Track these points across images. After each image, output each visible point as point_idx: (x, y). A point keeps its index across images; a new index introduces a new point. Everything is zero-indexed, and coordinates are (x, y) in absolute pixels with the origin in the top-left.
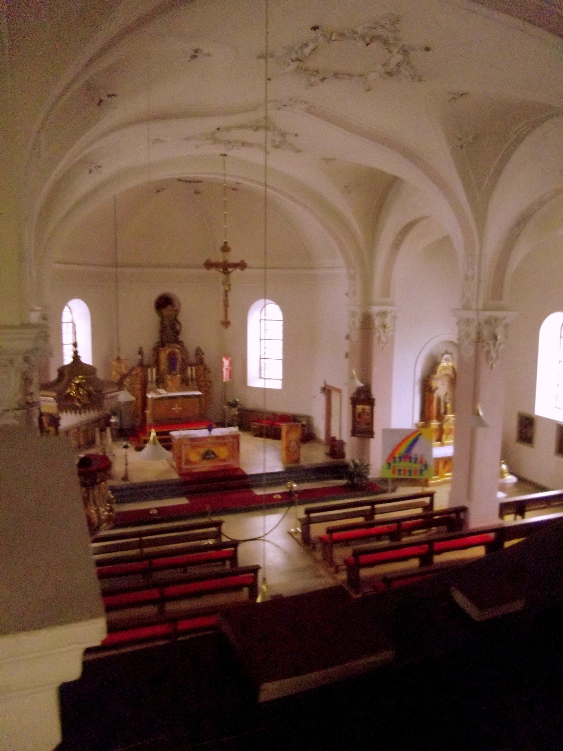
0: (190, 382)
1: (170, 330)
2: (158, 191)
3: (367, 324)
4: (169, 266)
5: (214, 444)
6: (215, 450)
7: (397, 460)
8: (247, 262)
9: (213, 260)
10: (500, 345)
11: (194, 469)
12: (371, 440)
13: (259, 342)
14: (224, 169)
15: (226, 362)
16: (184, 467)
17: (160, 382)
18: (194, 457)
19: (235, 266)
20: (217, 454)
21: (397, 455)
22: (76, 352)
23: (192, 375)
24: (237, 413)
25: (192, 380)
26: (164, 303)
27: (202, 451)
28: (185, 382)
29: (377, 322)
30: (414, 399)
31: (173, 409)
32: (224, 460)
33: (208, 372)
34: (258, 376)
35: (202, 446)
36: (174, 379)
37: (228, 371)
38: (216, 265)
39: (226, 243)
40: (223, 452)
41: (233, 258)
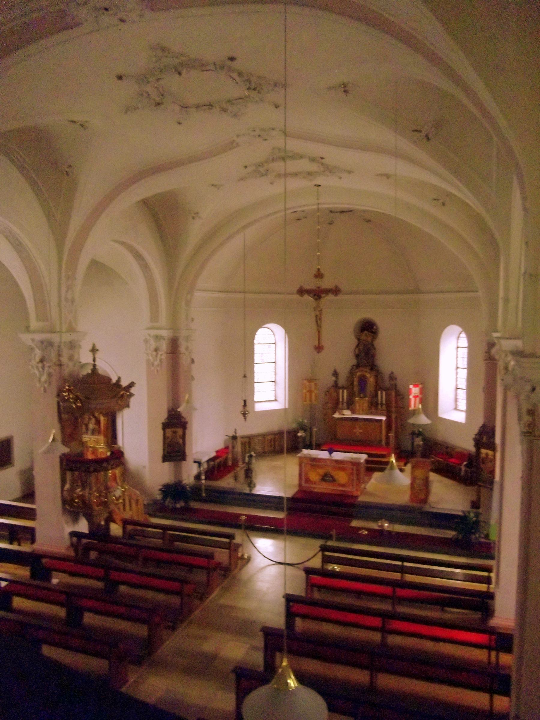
0: (379, 407)
1: (366, 354)
3: (174, 346)
4: (365, 293)
5: (335, 468)
6: (334, 473)
8: (341, 287)
9: (307, 287)
11: (315, 488)
12: (184, 462)
13: (455, 372)
14: (318, 199)
15: (415, 391)
16: (303, 484)
17: (350, 405)
18: (314, 476)
23: (382, 401)
24: (421, 443)
25: (382, 404)
26: (368, 328)
27: (321, 471)
28: (374, 406)
31: (355, 431)
32: (343, 485)
33: (403, 398)
34: (453, 406)
35: (320, 467)
36: (362, 403)
37: (418, 399)
38: (308, 292)
39: (319, 269)
40: (342, 477)
41: (326, 283)
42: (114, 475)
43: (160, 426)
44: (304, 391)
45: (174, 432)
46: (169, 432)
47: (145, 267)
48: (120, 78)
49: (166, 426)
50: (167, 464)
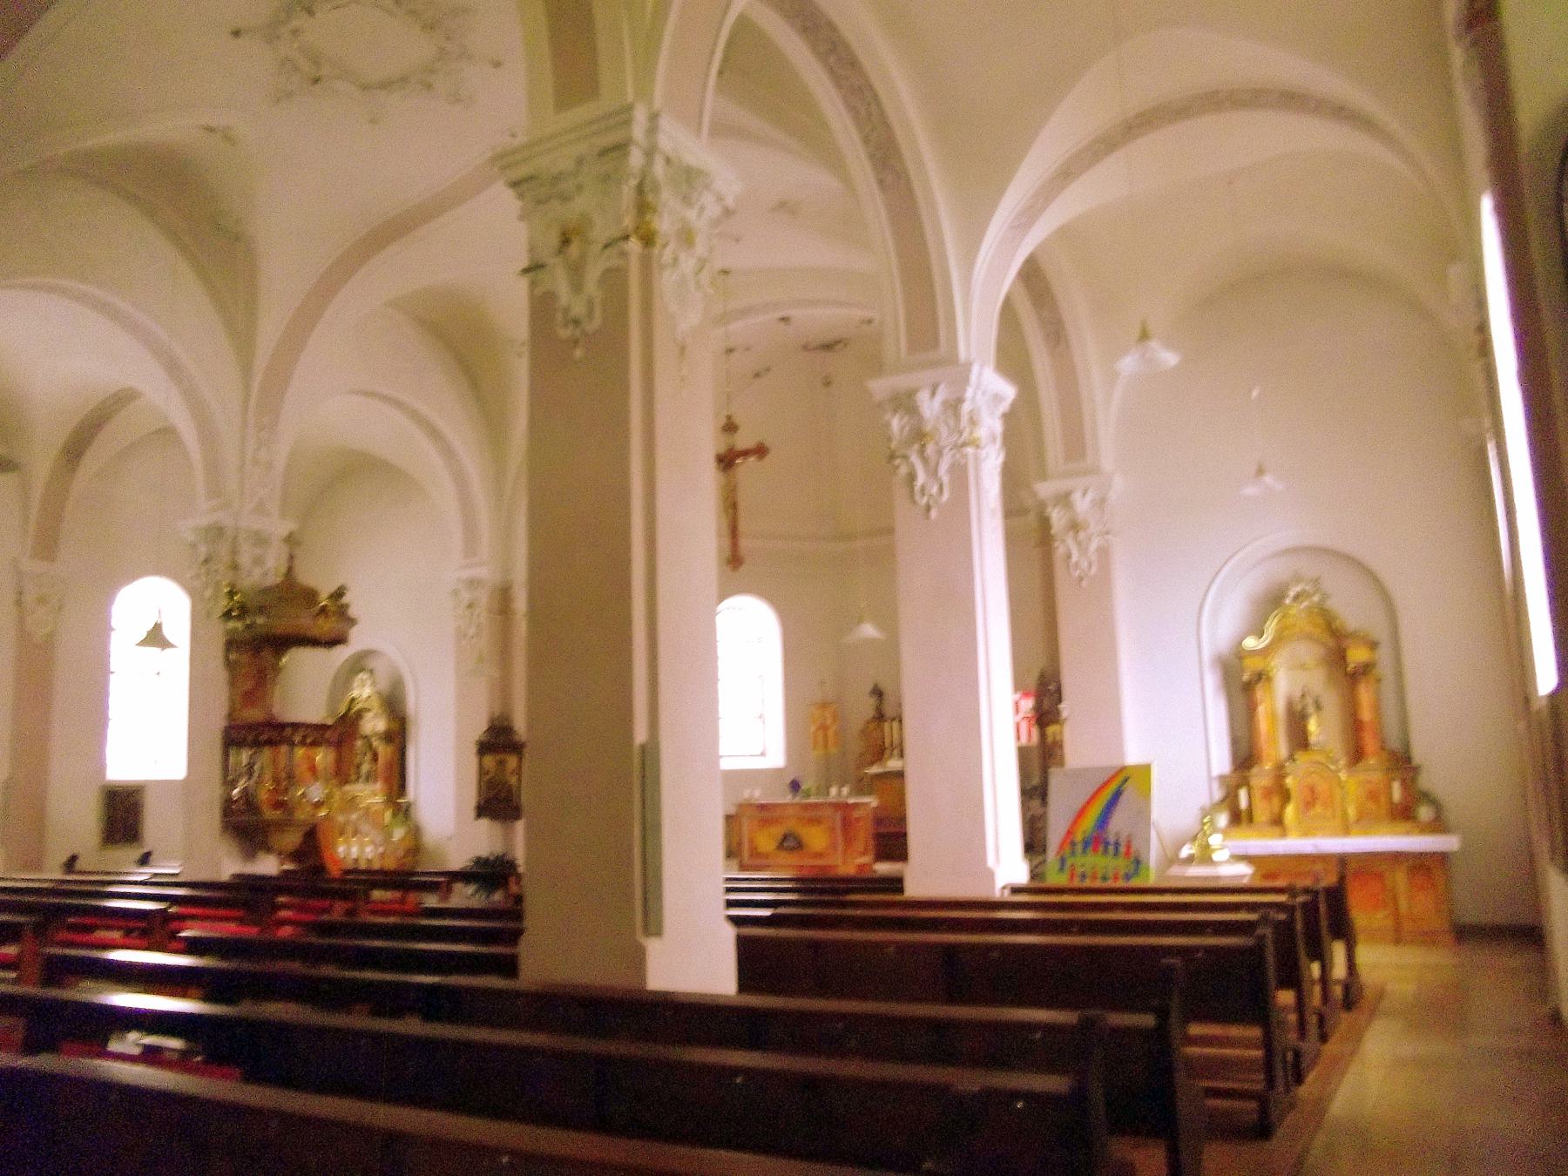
2: (757, 375)
7: (1079, 847)
10: (940, 453)
19: (745, 453)
20: (805, 840)
21: (1079, 837)
22: (290, 569)
27: (778, 831)
29: (1057, 517)
30: (1202, 680)
32: (820, 855)
41: (743, 441)
42: (311, 760)
43: (473, 749)
44: (813, 728)
45: (502, 763)
46: (489, 761)
47: (448, 452)
48: (236, 33)
49: (484, 748)
50: (485, 823)
